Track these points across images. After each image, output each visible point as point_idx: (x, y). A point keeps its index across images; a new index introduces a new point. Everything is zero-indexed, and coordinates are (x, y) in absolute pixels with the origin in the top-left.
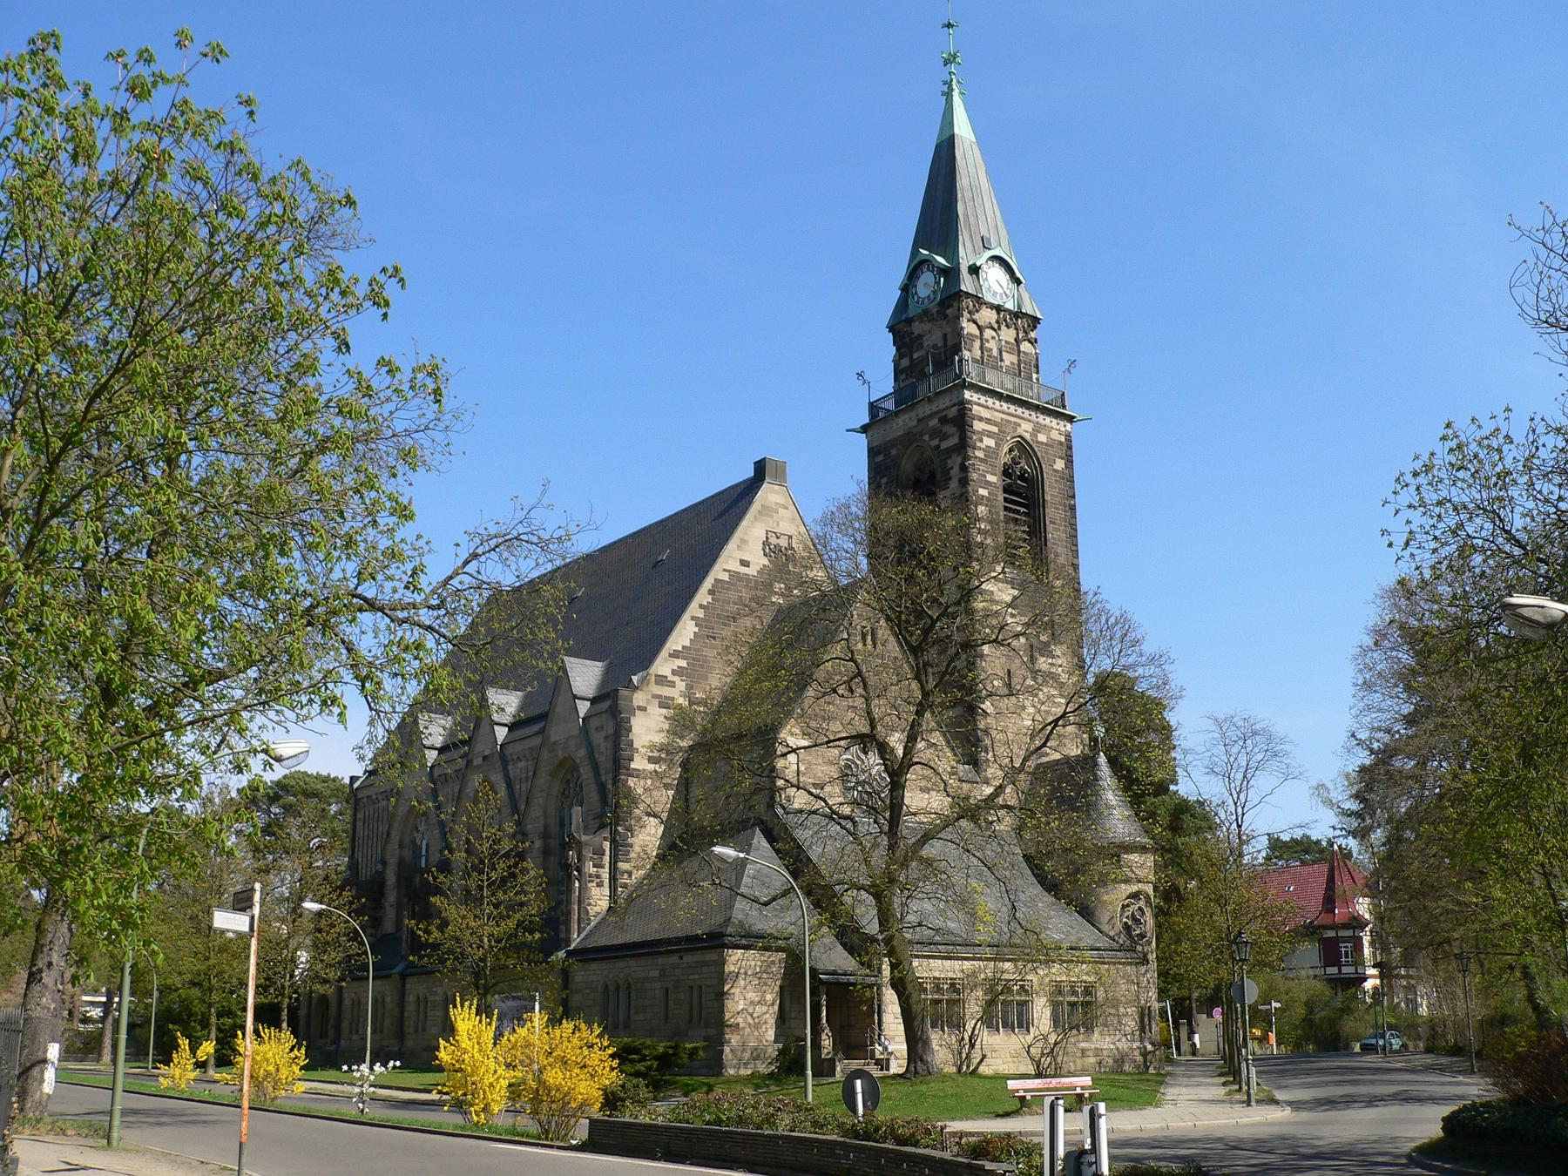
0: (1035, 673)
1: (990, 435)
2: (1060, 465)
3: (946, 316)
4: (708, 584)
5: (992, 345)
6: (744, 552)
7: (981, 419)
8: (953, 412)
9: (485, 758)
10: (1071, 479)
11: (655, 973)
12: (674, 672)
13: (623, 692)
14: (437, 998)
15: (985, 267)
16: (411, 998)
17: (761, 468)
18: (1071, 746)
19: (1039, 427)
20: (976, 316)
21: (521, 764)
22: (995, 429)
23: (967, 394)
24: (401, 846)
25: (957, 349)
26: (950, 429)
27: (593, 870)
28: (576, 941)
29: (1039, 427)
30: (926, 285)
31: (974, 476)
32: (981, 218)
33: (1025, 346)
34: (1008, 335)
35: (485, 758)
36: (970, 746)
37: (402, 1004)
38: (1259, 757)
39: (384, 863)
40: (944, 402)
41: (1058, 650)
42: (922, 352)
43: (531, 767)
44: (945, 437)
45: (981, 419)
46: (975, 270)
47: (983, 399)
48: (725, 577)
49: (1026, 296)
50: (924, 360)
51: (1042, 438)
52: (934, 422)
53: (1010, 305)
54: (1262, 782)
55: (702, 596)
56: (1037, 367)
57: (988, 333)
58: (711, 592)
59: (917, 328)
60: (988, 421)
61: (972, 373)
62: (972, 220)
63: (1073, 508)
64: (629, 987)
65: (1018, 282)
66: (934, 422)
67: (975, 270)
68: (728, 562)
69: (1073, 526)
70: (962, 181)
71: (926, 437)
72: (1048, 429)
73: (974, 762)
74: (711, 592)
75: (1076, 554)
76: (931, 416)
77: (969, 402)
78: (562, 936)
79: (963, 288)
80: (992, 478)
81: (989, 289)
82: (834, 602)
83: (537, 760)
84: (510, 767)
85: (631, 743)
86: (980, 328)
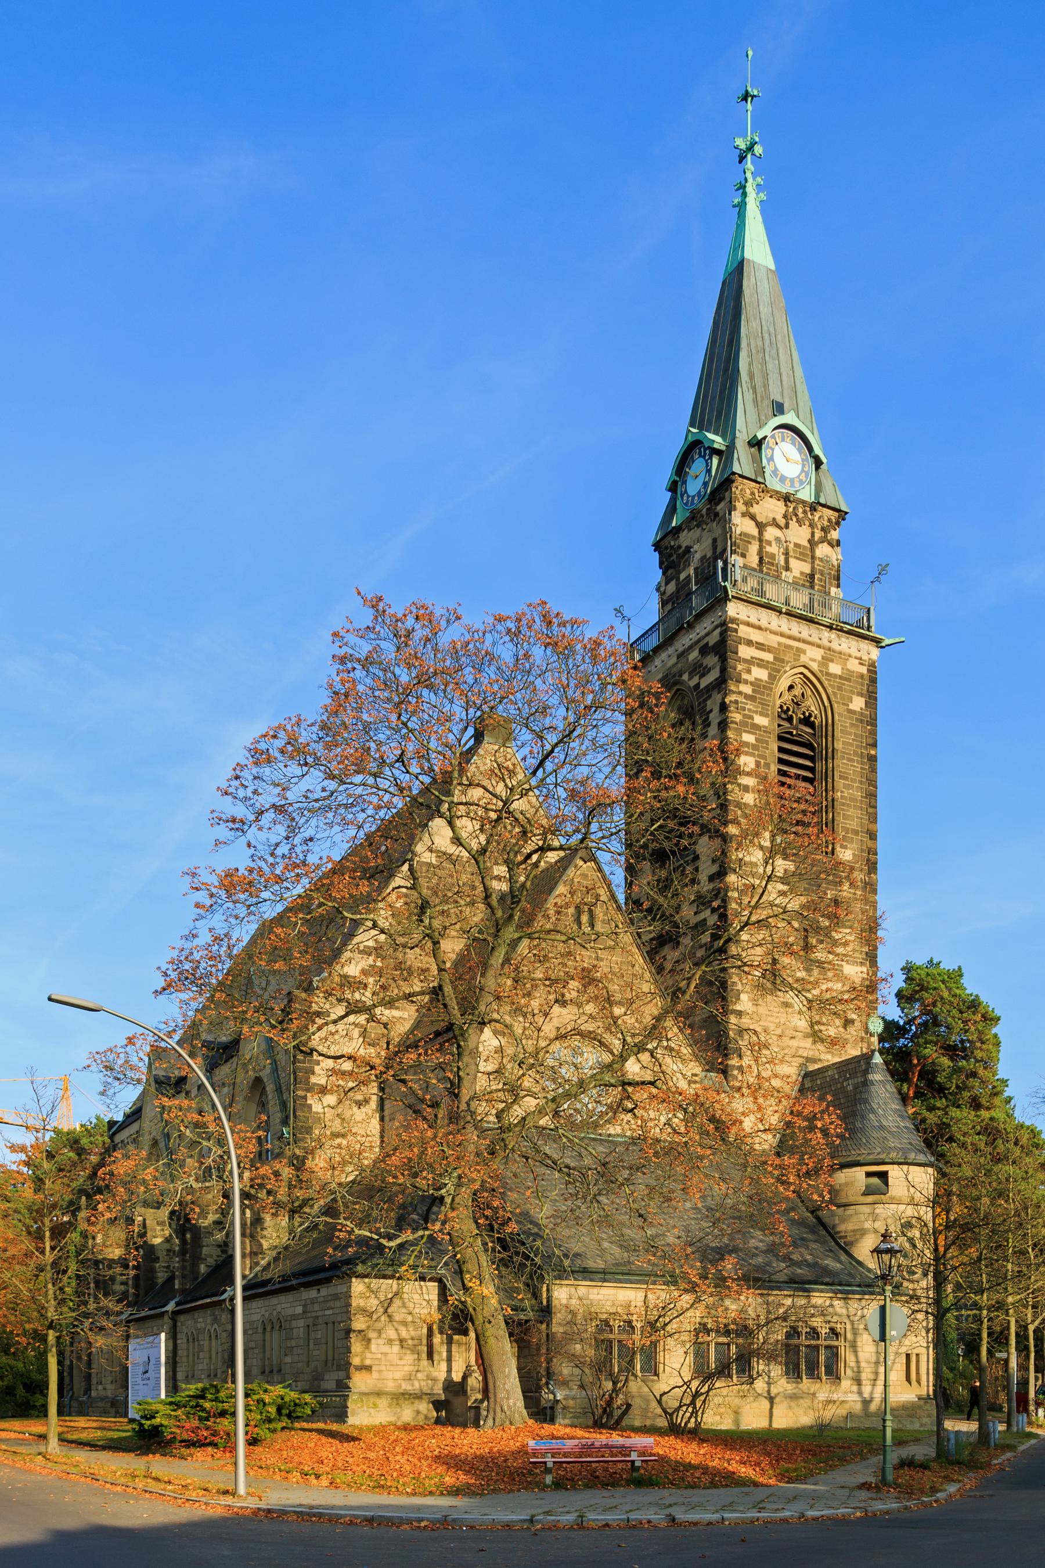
1: (761, 664)
2: (858, 704)
3: (717, 514)
7: (749, 643)
8: (714, 638)
10: (873, 722)
11: (299, 1310)
12: (364, 972)
20: (755, 509)
29: (830, 655)
31: (737, 717)
32: (773, 377)
33: (823, 550)
34: (799, 534)
40: (706, 625)
44: (705, 672)
45: (749, 643)
46: (757, 444)
49: (828, 483)
51: (835, 668)
52: (694, 655)
57: (771, 533)
59: (685, 539)
60: (760, 646)
62: (758, 380)
63: (873, 759)
65: (818, 463)
69: (872, 782)
71: (685, 677)
72: (843, 657)
75: (873, 818)
76: (691, 648)
77: (734, 620)
79: (736, 468)
80: (761, 721)
81: (775, 472)
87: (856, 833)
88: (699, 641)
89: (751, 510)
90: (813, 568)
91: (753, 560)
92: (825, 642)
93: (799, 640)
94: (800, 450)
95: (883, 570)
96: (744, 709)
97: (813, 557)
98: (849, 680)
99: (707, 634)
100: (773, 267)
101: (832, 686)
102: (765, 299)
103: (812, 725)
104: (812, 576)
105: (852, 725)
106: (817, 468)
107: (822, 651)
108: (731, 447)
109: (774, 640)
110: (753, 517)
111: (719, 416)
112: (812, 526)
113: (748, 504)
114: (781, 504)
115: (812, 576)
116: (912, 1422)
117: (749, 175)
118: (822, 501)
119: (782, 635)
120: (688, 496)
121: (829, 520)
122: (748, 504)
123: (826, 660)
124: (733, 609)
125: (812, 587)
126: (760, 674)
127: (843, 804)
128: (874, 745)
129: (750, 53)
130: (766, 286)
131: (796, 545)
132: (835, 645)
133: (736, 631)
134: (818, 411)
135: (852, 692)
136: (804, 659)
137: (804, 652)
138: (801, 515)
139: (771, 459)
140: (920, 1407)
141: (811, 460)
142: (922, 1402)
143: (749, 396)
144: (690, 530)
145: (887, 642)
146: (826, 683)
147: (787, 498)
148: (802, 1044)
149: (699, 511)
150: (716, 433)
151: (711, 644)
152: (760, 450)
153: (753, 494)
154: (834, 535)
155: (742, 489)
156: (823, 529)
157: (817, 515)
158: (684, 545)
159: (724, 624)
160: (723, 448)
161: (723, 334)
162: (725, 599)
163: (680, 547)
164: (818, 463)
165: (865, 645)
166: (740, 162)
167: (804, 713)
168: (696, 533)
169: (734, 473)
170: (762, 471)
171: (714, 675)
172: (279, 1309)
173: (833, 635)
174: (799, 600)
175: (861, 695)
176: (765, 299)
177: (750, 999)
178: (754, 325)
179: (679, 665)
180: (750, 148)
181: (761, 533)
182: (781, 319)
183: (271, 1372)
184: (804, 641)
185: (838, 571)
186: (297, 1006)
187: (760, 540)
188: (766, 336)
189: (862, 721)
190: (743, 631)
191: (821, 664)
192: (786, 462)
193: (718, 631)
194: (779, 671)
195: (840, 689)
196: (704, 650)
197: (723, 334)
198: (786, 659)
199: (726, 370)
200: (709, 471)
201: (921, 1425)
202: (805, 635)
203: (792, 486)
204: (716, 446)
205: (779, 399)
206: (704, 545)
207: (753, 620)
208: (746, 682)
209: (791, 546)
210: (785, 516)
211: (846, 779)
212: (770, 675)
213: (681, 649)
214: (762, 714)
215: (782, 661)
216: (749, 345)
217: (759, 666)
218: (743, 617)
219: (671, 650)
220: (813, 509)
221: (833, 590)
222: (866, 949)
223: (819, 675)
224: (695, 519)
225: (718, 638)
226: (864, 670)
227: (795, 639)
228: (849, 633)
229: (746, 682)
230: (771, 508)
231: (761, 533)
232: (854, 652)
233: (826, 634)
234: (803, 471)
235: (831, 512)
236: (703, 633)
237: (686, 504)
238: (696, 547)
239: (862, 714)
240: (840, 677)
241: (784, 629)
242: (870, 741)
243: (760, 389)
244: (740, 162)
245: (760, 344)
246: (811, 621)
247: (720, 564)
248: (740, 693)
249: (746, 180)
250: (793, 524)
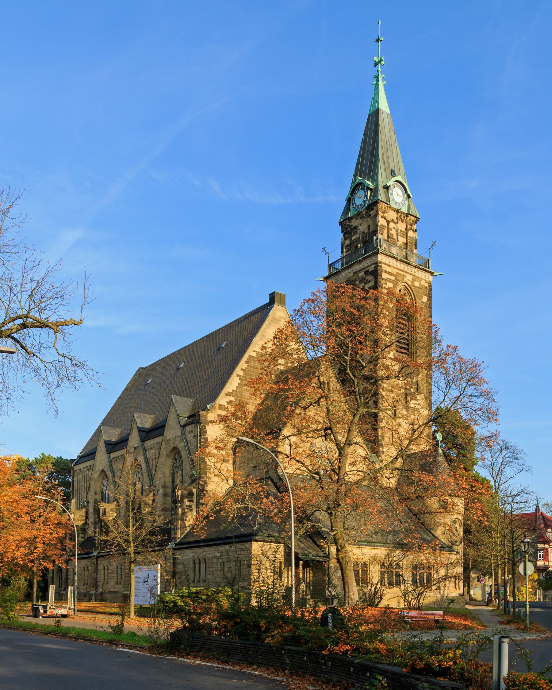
1: (390, 281)
2: (425, 299)
3: (370, 215)
4: (245, 358)
5: (393, 232)
6: (264, 340)
7: (386, 272)
8: (372, 268)
9: (135, 448)
10: (430, 307)
12: (228, 403)
13: (202, 413)
14: (113, 567)
15: (392, 187)
16: (100, 568)
17: (273, 298)
18: (422, 446)
20: (386, 215)
21: (153, 451)
22: (393, 278)
23: (381, 258)
24: (96, 494)
25: (375, 232)
26: (370, 278)
27: (188, 503)
28: (179, 535)
29: (415, 278)
30: (360, 199)
32: (391, 159)
33: (410, 234)
34: (402, 226)
35: (135, 448)
36: (374, 444)
37: (96, 571)
38: (508, 459)
39: (88, 502)
42: (356, 236)
43: (157, 452)
44: (367, 282)
45: (386, 272)
46: (387, 188)
48: (254, 354)
49: (412, 206)
50: (357, 240)
51: (417, 284)
52: (361, 274)
53: (404, 210)
54: (508, 471)
55: (243, 364)
56: (416, 245)
57: (392, 225)
58: (247, 362)
59: (354, 223)
60: (390, 274)
61: (383, 246)
62: (386, 160)
64: (205, 562)
65: (409, 197)
66: (361, 274)
67: (387, 188)
68: (255, 348)
70: (382, 138)
72: (419, 279)
73: (377, 453)
74: (247, 362)
77: (380, 262)
78: (172, 536)
79: (380, 198)
81: (393, 200)
82: (305, 371)
83: (160, 448)
84: (147, 453)
85: (206, 439)
88: (364, 268)
89: (385, 215)
90: (407, 241)
91: (385, 236)
92: (413, 273)
94: (402, 191)
95: (434, 244)
97: (407, 236)
98: (421, 289)
99: (368, 266)
100: (389, 113)
102: (387, 126)
104: (406, 244)
106: (408, 198)
108: (376, 188)
109: (395, 271)
110: (385, 218)
111: (369, 173)
112: (406, 223)
113: (384, 213)
114: (395, 213)
115: (406, 244)
116: (457, 605)
117: (379, 73)
118: (411, 213)
119: (398, 269)
120: (356, 205)
121: (413, 221)
122: (384, 213)
123: (414, 280)
124: (381, 258)
125: (406, 249)
126: (390, 285)
128: (431, 317)
129: (380, 22)
130: (387, 120)
131: (401, 231)
132: (416, 274)
133: (381, 267)
134: (408, 175)
135: (423, 294)
136: (405, 279)
137: (406, 276)
138: (403, 218)
139: (392, 194)
140: (460, 599)
141: (406, 196)
142: (460, 597)
143: (382, 167)
144: (357, 219)
145: (436, 274)
146: (413, 290)
147: (398, 211)
149: (362, 212)
150: (369, 181)
151: (370, 271)
152: (388, 190)
153: (385, 208)
154: (414, 227)
155: (382, 206)
157: (408, 218)
158: (354, 226)
159: (376, 263)
160: (373, 188)
161: (370, 138)
162: (377, 253)
163: (352, 226)
164: (409, 197)
165: (427, 275)
166: (375, 66)
168: (360, 221)
169: (379, 200)
170: (388, 199)
171: (372, 284)
172: (204, 553)
173: (416, 270)
174: (402, 253)
175: (426, 295)
176: (387, 126)
178: (383, 136)
179: (354, 277)
180: (380, 62)
181: (388, 225)
182: (393, 135)
183: (199, 581)
184: (406, 272)
185: (416, 242)
187: (388, 228)
188: (388, 142)
189: (426, 306)
190: (384, 267)
192: (397, 196)
193: (373, 266)
194: (396, 284)
195: (418, 292)
196: (367, 273)
197: (370, 138)
199: (372, 154)
200: (366, 196)
201: (461, 606)
202: (406, 270)
203: (399, 206)
204: (370, 187)
205: (393, 169)
206: (363, 227)
207: (387, 262)
208: (385, 288)
209: (399, 231)
210: (397, 218)
213: (355, 271)
215: (398, 280)
216: (382, 145)
217: (390, 282)
218: (383, 261)
219: (350, 270)
220: (407, 216)
221: (414, 250)
223: (411, 286)
224: (358, 215)
225: (373, 269)
226: (427, 285)
228: (422, 269)
230: (392, 215)
231: (388, 225)
233: (414, 269)
235: (413, 218)
236: (366, 265)
237: (355, 208)
238: (360, 227)
239: (426, 303)
240: (419, 288)
241: (399, 267)
242: (429, 315)
243: (386, 164)
244: (375, 66)
245: (386, 145)
246: (409, 264)
247: (375, 238)
249: (378, 75)
250: (400, 222)
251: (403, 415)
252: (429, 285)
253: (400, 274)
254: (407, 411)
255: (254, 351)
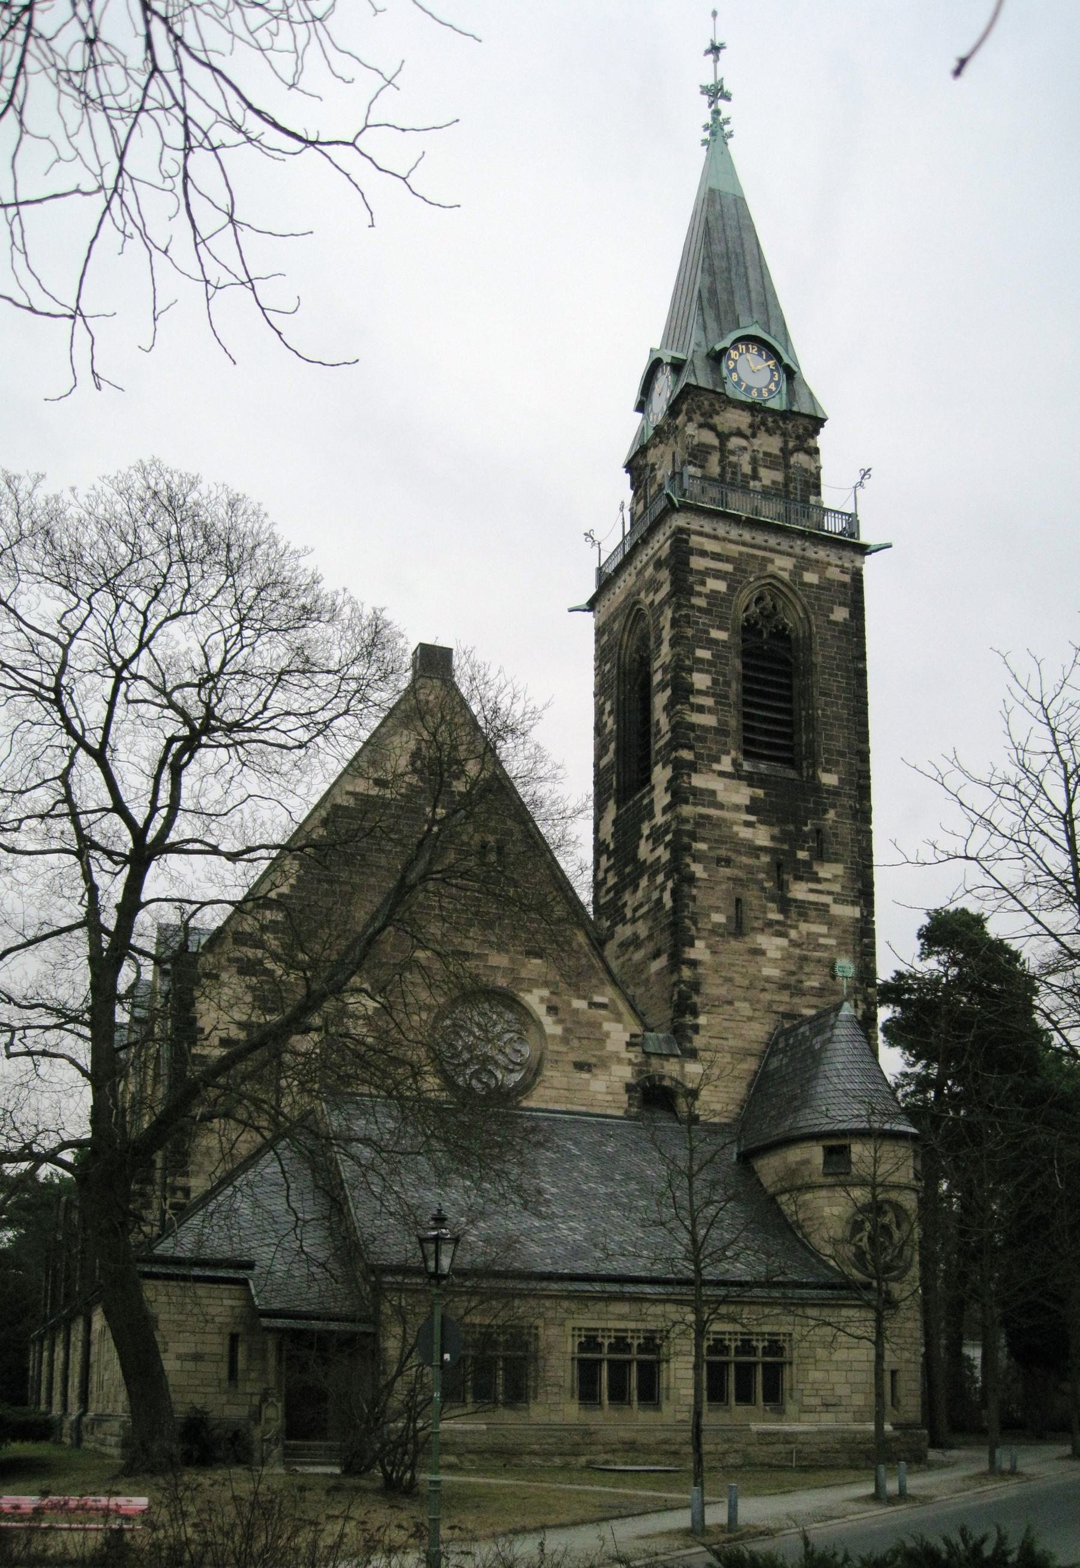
0: (785, 904)
7: (703, 554)
19: (804, 564)
20: (716, 420)
22: (729, 567)
34: (772, 444)
41: (826, 871)
45: (703, 554)
47: (707, 526)
51: (810, 577)
52: (650, 570)
53: (775, 404)
60: (716, 557)
86: (719, 435)
87: (842, 754)
92: (797, 550)
93: (765, 549)
96: (697, 623)
101: (808, 597)
103: (787, 639)
105: (833, 637)
107: (794, 560)
109: (734, 550)
110: (713, 428)
112: (784, 434)
123: (798, 571)
127: (825, 723)
136: (770, 568)
137: (772, 561)
138: (770, 424)
148: (777, 998)
156: (798, 437)
167: (776, 627)
174: (770, 511)
175: (842, 604)
177: (708, 947)
184: (772, 550)
186: (661, 1035)
189: (846, 633)
191: (791, 573)
195: (818, 599)
198: (749, 569)
208: (700, 594)
211: (829, 695)
212: (729, 587)
214: (720, 628)
215: (745, 571)
222: (859, 885)
226: (847, 578)
227: (759, 548)
229: (700, 594)
232: (834, 559)
234: (771, 381)
240: (818, 587)
248: (693, 607)
251: (770, 924)
252: (853, 579)
253: (754, 556)
254: (783, 910)
255: (348, 793)
